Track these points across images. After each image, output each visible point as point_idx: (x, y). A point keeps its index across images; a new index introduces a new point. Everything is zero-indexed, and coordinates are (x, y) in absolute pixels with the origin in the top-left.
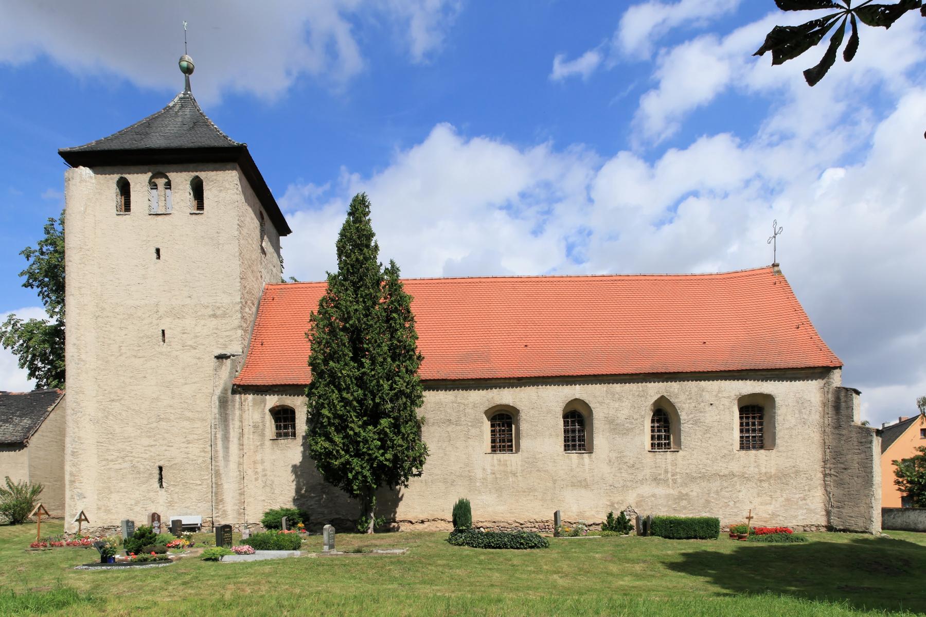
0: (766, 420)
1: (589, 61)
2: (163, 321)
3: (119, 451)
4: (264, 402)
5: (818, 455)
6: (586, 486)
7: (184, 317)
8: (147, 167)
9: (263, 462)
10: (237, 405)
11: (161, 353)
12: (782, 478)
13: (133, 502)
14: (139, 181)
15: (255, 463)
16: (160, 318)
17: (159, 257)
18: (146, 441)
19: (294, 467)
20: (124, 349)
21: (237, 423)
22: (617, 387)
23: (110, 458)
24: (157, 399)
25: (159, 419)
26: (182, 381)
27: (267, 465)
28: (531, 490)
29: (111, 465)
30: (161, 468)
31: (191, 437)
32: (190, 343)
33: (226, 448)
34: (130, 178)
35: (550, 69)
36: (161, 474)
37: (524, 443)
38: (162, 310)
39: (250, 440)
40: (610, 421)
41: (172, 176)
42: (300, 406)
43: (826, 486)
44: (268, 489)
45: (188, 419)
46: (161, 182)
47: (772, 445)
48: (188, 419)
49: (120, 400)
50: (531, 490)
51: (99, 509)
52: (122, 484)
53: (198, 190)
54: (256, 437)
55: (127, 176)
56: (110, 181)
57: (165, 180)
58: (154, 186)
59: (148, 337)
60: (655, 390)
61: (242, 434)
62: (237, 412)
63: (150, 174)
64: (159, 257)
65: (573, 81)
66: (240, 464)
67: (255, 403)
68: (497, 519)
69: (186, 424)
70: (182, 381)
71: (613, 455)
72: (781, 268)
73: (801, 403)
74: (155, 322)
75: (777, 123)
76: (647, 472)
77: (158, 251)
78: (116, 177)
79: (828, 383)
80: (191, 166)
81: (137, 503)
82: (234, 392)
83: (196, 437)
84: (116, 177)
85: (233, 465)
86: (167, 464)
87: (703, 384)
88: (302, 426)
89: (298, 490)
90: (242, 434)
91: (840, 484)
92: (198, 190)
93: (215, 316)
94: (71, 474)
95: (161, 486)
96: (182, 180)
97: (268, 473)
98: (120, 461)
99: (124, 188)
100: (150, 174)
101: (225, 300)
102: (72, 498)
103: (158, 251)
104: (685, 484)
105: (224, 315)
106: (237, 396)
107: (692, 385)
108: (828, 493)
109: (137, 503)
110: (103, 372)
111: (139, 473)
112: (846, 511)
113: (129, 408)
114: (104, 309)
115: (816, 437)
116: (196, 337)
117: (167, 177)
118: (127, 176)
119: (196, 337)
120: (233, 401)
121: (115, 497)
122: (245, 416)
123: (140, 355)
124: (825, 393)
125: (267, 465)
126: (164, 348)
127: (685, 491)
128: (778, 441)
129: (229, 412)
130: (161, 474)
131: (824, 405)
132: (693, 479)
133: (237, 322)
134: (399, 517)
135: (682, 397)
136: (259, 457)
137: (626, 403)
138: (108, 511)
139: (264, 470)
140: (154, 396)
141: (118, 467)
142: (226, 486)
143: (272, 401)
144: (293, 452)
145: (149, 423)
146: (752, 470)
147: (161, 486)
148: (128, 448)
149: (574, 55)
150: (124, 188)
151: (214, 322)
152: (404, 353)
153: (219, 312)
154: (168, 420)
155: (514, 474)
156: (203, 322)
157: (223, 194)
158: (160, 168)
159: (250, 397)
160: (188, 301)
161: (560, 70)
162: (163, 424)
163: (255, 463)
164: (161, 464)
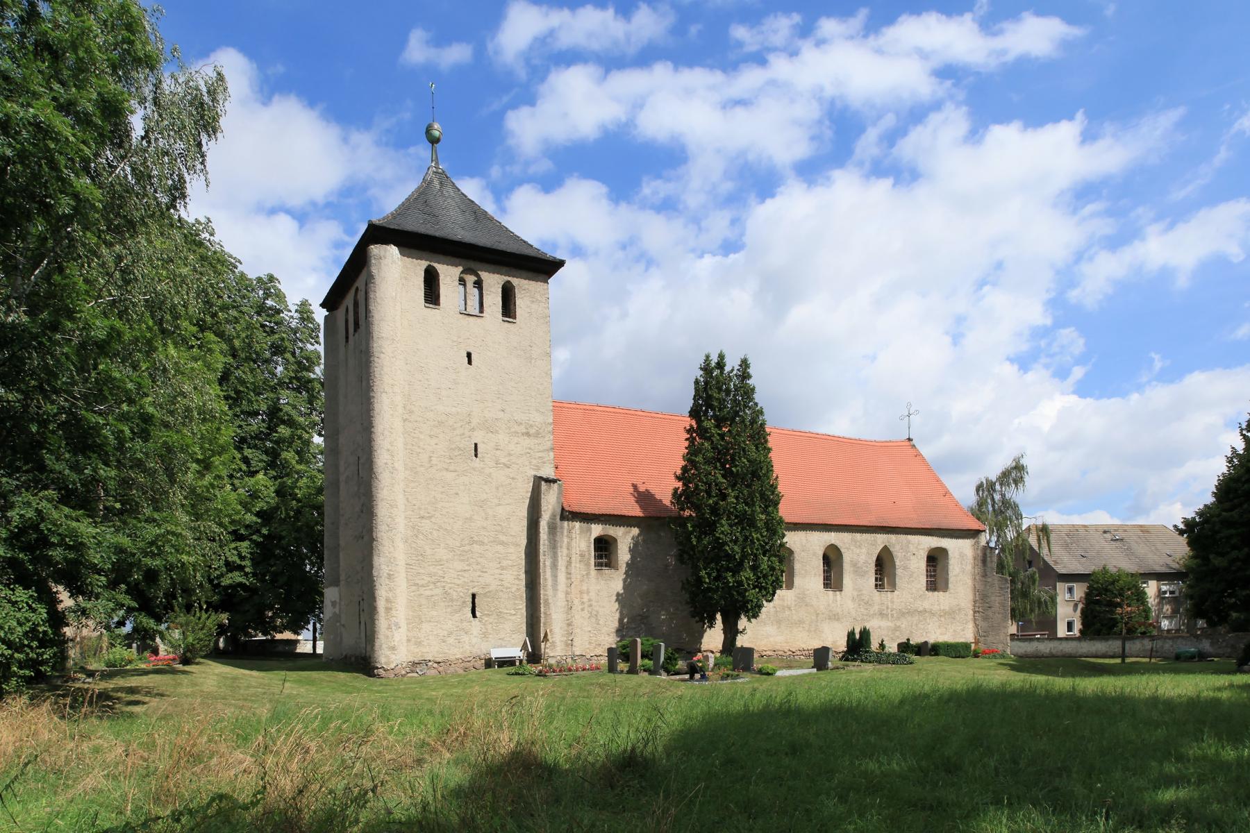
0: (939, 568)
1: (457, 54)
2: (475, 433)
3: (430, 575)
4: (590, 530)
5: (970, 597)
6: (838, 620)
7: (497, 432)
8: (458, 260)
9: (588, 592)
10: (565, 533)
11: (474, 469)
12: (951, 614)
13: (446, 633)
14: (449, 274)
15: (581, 592)
16: (473, 430)
17: (470, 362)
18: (459, 565)
19: (618, 595)
20: (434, 461)
21: (565, 551)
22: (858, 536)
23: (421, 582)
24: (470, 519)
25: (473, 542)
26: (496, 501)
27: (593, 595)
28: (801, 622)
29: (422, 590)
30: (474, 596)
31: (505, 563)
32: (503, 460)
33: (555, 576)
34: (442, 269)
35: (403, 43)
36: (473, 603)
37: (797, 581)
38: (475, 422)
39: (578, 568)
40: (854, 565)
41: (484, 275)
42: (625, 538)
43: (975, 620)
44: (593, 620)
45: (502, 543)
46: (470, 279)
47: (945, 588)
48: (502, 543)
49: (430, 517)
50: (801, 622)
51: (409, 641)
52: (435, 613)
53: (508, 296)
54: (582, 566)
55: (438, 267)
56: (416, 268)
57: (474, 278)
58: (462, 281)
59: (460, 449)
60: (881, 540)
61: (569, 563)
62: (566, 540)
63: (461, 269)
64: (470, 362)
65: (430, 71)
66: (567, 593)
67: (582, 531)
68: (777, 648)
69: (500, 548)
70: (496, 501)
71: (855, 593)
72: (914, 442)
73: (962, 555)
74: (467, 434)
75: (651, 188)
76: (876, 608)
77: (469, 355)
78: (424, 264)
79: (978, 543)
80: (504, 269)
81: (450, 634)
82: (563, 518)
83: (510, 563)
84: (424, 264)
85: (561, 595)
86: (481, 591)
87: (909, 537)
88: (623, 555)
89: (621, 621)
90: (569, 563)
91: (985, 619)
92: (508, 296)
93: (528, 434)
94: (388, 600)
95: (474, 616)
96: (494, 282)
97: (594, 603)
98: (432, 586)
99: (431, 280)
100: (461, 269)
101: (537, 419)
102: (389, 628)
103: (469, 355)
104: (898, 619)
105: (537, 435)
106: (566, 523)
107: (902, 537)
108: (976, 625)
109: (450, 634)
110: (413, 485)
111: (452, 600)
112: (989, 639)
113: (440, 527)
114: (411, 412)
115: (970, 582)
116: (510, 455)
117: (477, 275)
118: (438, 267)
119: (510, 455)
120: (562, 528)
121: (426, 627)
122: (573, 544)
123: (452, 468)
124: (975, 550)
125: (593, 595)
126: (476, 463)
127: (898, 624)
128: (950, 585)
129: (558, 538)
130: (473, 603)
131: (975, 559)
132: (903, 614)
133: (549, 444)
134: (703, 647)
135: (897, 547)
136: (585, 588)
137: (864, 550)
138: (418, 643)
139: (590, 600)
140: (467, 515)
141: (428, 593)
142: (554, 616)
143: (597, 530)
144: (615, 582)
145: (462, 546)
146: (936, 608)
147: (474, 616)
148: (440, 573)
149: (441, 40)
150: (431, 280)
151: (527, 442)
152: (770, 500)
153: (532, 431)
154: (482, 543)
155: (789, 608)
156: (516, 440)
157: (534, 306)
158: (472, 265)
159: (577, 524)
160: (501, 415)
161: (417, 50)
162: (476, 547)
163: (581, 592)
164: (474, 591)
